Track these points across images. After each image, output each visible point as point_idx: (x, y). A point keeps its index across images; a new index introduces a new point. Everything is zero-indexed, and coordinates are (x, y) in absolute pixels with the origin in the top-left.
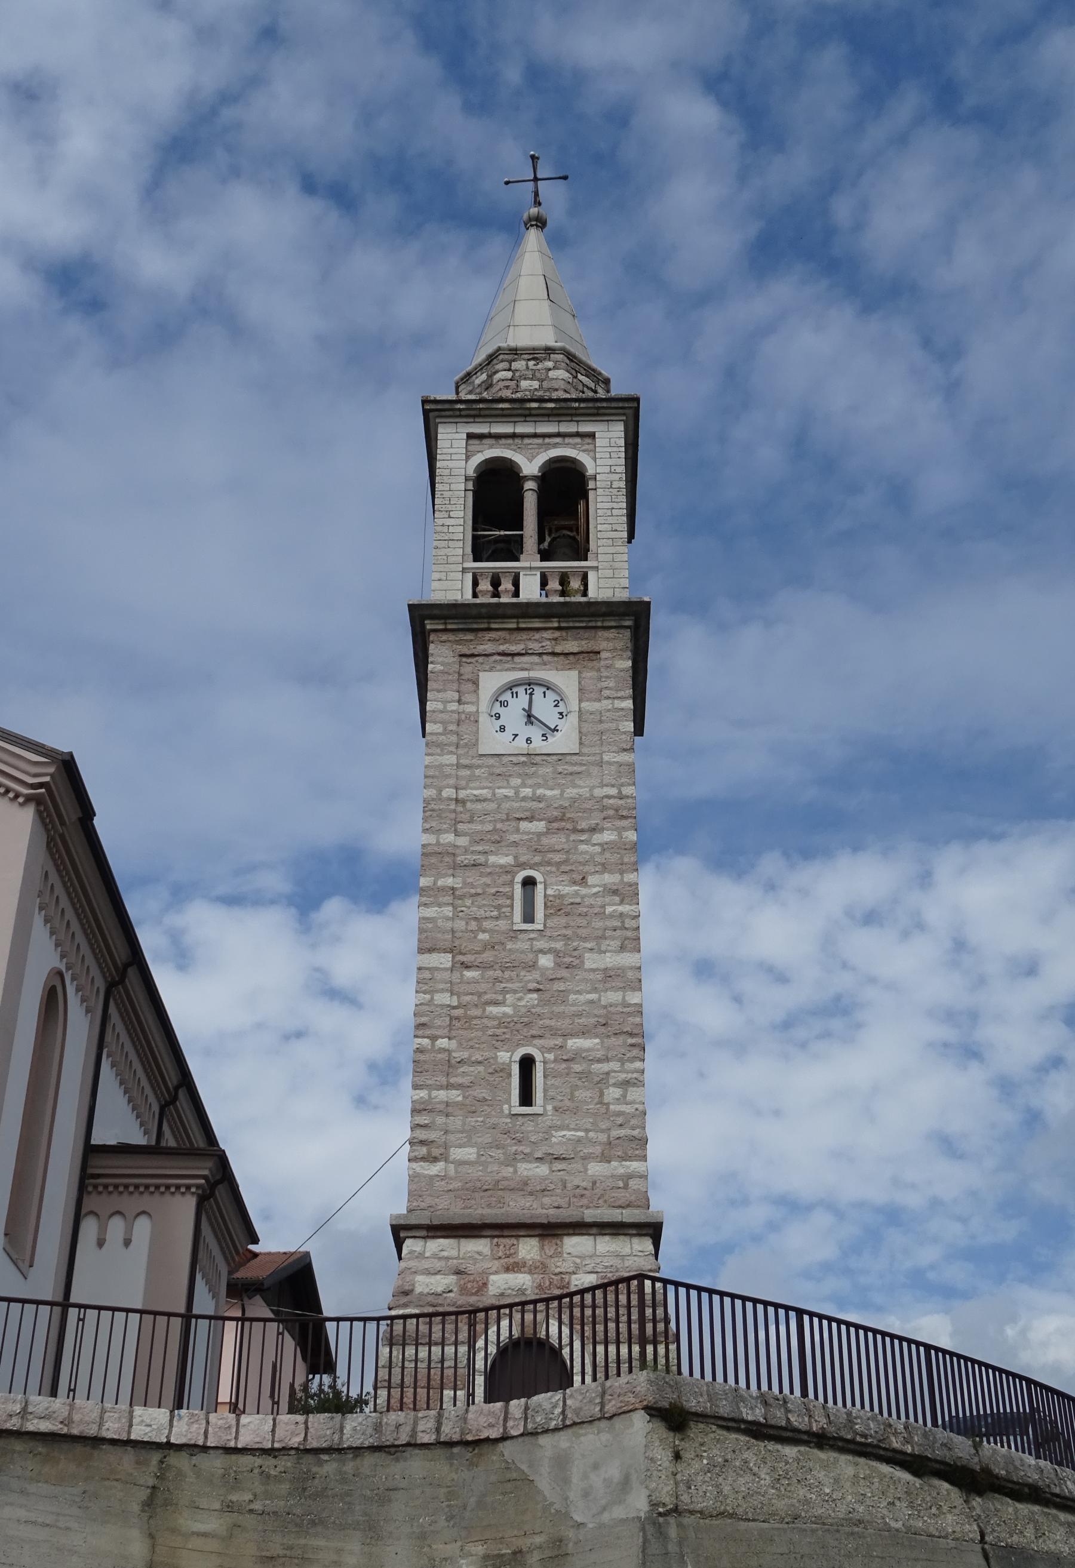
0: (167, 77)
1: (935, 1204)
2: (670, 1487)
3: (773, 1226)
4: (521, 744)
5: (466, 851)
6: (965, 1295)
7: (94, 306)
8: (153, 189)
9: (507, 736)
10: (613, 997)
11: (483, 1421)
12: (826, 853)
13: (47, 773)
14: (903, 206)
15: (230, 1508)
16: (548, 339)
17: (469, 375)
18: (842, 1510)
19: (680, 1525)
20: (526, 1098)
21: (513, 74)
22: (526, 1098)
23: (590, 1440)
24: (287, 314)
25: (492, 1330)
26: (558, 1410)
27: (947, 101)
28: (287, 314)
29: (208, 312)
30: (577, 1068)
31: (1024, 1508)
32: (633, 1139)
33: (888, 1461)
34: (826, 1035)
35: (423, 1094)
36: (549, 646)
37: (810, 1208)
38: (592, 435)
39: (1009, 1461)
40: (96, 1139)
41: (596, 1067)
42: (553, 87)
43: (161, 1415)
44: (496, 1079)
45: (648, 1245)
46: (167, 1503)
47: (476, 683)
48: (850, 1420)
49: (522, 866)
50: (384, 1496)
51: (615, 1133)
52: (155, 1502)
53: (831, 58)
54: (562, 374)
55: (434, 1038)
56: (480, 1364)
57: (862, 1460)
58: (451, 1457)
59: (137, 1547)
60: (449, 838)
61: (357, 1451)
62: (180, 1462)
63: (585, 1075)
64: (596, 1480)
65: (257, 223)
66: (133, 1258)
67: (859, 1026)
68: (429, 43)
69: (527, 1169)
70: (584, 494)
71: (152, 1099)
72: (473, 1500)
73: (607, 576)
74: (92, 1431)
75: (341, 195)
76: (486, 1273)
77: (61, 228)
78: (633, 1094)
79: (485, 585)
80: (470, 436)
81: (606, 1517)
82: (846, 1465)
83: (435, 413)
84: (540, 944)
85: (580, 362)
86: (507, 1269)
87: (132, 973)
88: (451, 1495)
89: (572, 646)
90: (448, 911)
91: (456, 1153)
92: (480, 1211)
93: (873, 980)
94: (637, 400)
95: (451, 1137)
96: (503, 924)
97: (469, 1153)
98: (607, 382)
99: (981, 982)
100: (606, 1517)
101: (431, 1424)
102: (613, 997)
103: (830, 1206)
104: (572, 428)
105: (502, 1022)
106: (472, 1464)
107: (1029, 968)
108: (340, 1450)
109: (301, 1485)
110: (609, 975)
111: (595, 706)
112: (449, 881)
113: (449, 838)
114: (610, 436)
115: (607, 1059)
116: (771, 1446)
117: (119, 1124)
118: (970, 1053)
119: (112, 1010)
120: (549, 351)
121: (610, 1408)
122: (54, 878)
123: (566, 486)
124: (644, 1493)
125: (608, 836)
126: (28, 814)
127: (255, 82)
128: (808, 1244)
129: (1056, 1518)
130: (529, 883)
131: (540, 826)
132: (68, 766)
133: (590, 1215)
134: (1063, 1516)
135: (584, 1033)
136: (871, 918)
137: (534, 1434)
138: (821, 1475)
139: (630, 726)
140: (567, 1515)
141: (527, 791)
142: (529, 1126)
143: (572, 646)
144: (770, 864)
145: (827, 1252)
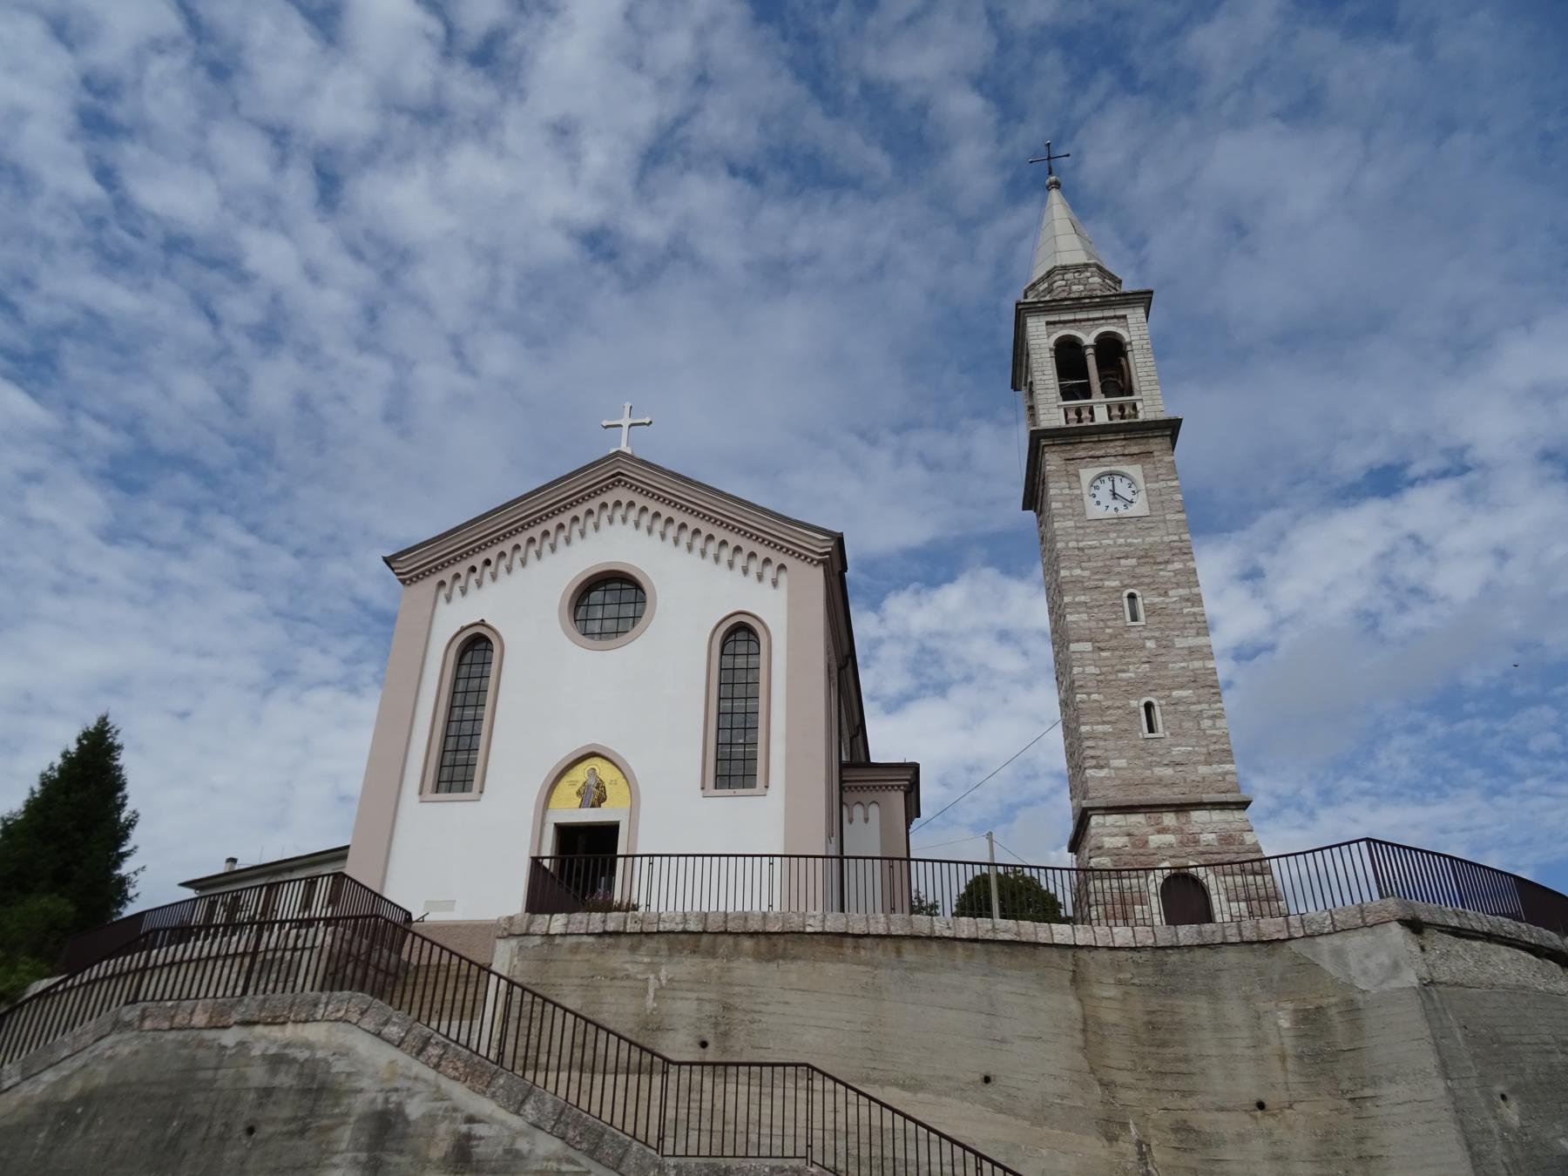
0: (644, 113)
4: (1111, 512)
7: (611, 256)
8: (640, 181)
9: (1102, 507)
10: (1197, 664)
13: (829, 546)
15: (1120, 982)
16: (1081, 258)
21: (852, 90)
22: (1151, 729)
24: (726, 251)
26: (1328, 922)
27: (1128, 81)
28: (726, 251)
32: (1224, 750)
42: (877, 96)
44: (1131, 717)
46: (1083, 980)
47: (1078, 476)
49: (1126, 587)
50: (1215, 974)
51: (1212, 747)
52: (1077, 979)
53: (1051, 59)
54: (1096, 280)
55: (1089, 694)
58: (1253, 951)
59: (1075, 1007)
60: (1078, 572)
61: (1190, 947)
62: (1083, 955)
64: (1371, 964)
65: (704, 197)
68: (799, 76)
70: (1125, 354)
72: (1276, 977)
74: (1033, 939)
76: (1146, 835)
77: (588, 211)
78: (1219, 723)
79: (1072, 415)
80: (1048, 323)
81: (1385, 987)
82: (1506, 953)
84: (1146, 634)
86: (1159, 832)
88: (1260, 973)
89: (1135, 449)
90: (1085, 617)
91: (1115, 763)
92: (1136, 798)
95: (1110, 754)
96: (1120, 623)
97: (1122, 763)
100: (1385, 987)
101: (1235, 931)
102: (1197, 664)
105: (1129, 682)
109: (1160, 968)
110: (1191, 651)
111: (1156, 486)
112: (1083, 598)
113: (1078, 572)
115: (1199, 703)
120: (1087, 266)
123: (1112, 350)
124: (1413, 973)
125: (1177, 566)
126: (820, 571)
127: (696, 110)
130: (1132, 597)
131: (1133, 561)
133: (1206, 798)
135: (1182, 687)
137: (1312, 936)
140: (1352, 985)
141: (1121, 541)
142: (1157, 745)
143: (1135, 449)
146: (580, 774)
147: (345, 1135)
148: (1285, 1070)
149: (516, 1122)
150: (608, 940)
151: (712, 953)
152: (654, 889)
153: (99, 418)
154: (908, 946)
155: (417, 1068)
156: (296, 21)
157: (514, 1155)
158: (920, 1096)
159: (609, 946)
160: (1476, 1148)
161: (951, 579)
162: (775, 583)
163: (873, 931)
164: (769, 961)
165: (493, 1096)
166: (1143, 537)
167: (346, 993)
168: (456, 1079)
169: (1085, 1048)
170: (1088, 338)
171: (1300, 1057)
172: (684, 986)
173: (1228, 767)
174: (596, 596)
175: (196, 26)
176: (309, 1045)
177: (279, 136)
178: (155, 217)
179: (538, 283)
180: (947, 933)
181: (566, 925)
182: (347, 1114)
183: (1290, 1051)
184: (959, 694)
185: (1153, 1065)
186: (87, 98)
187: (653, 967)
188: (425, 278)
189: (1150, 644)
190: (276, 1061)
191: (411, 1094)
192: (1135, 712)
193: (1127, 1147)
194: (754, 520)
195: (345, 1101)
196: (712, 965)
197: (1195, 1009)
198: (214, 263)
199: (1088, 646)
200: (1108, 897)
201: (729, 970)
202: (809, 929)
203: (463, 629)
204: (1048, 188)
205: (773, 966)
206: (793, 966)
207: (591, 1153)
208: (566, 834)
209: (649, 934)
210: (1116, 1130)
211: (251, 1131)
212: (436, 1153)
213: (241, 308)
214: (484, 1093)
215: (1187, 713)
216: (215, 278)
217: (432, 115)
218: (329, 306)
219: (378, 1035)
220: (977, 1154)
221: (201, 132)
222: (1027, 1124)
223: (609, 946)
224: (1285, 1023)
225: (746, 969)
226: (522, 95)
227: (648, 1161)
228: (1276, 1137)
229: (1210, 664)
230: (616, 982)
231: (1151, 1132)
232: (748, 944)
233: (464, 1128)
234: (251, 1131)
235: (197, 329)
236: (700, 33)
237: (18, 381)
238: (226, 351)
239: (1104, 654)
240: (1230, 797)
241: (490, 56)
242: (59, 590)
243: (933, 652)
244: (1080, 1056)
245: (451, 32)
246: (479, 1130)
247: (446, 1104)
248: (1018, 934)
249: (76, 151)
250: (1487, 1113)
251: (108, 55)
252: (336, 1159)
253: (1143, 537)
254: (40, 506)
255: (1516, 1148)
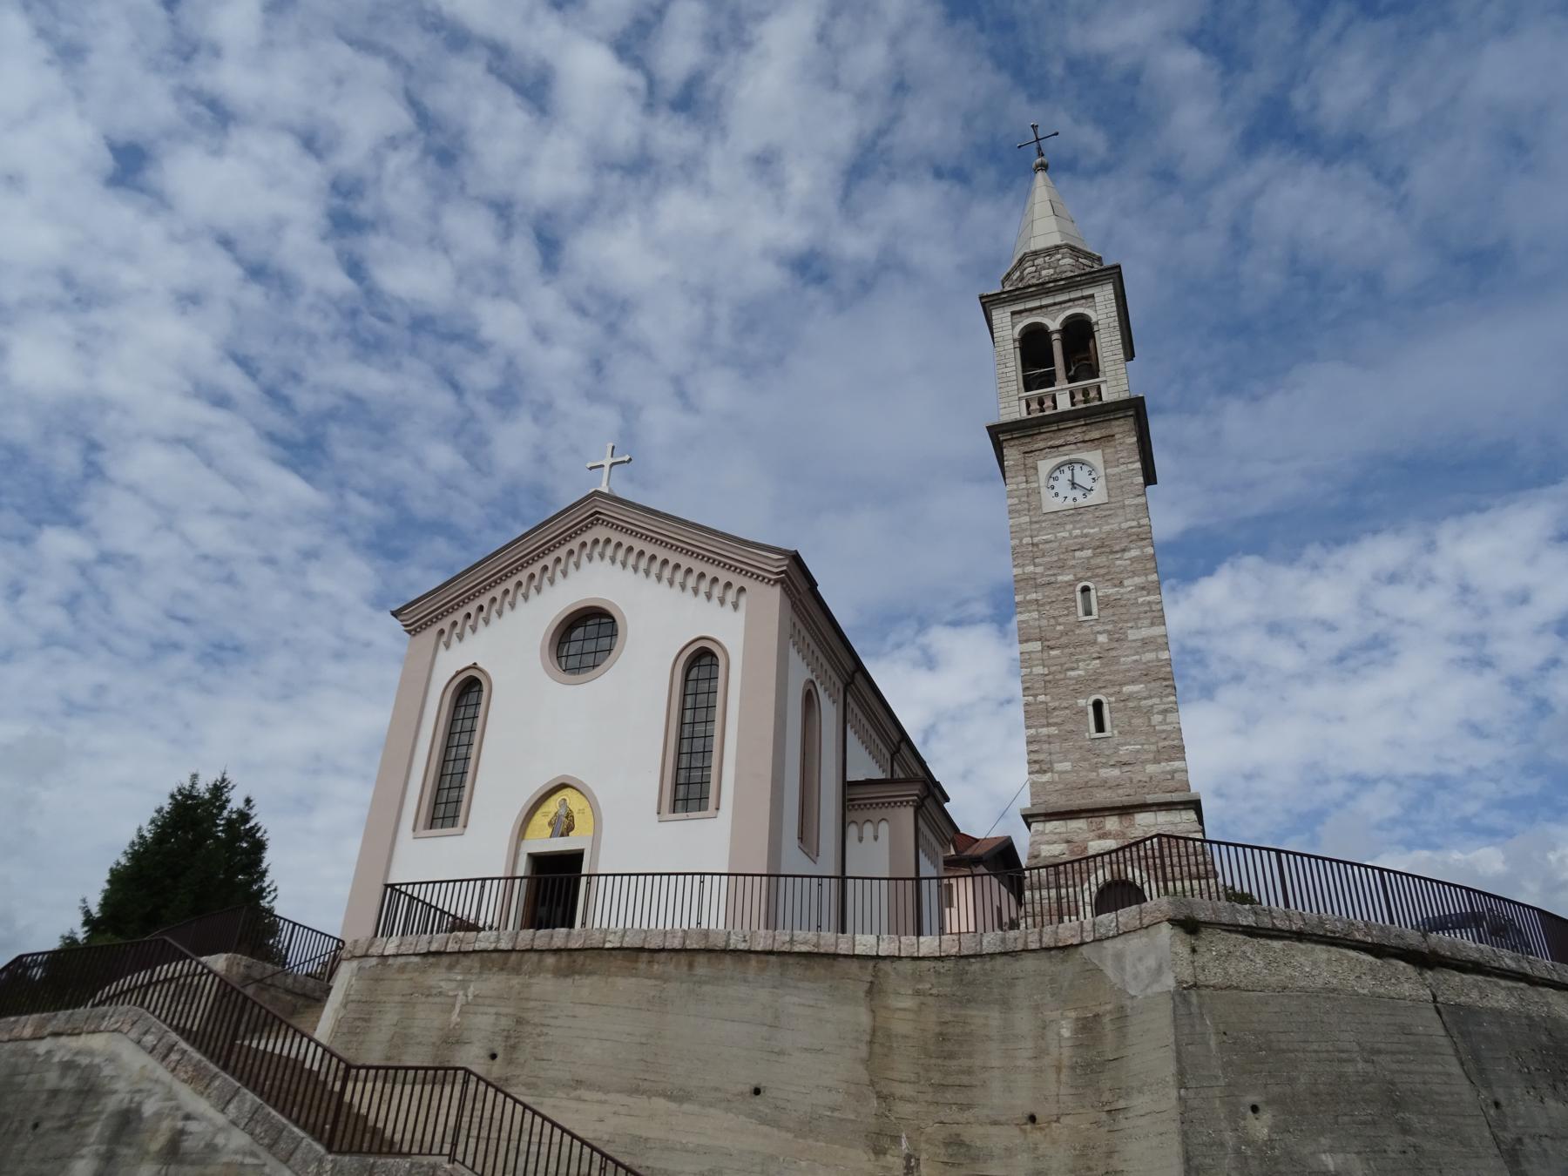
0: (841, 130)
1: (1472, 772)
2: (1190, 970)
3: (1350, 796)
4: (1070, 502)
5: (1043, 575)
6: (1509, 834)
7: (821, 279)
9: (1060, 499)
11: (1068, 933)
12: (1355, 539)
13: (784, 564)
14: (1344, 86)
15: (917, 993)
17: (1009, 275)
18: (1319, 982)
19: (1199, 996)
20: (1100, 727)
21: (1057, 69)
22: (1100, 727)
23: (1136, 942)
25: (1093, 878)
29: (889, 266)
30: (1131, 704)
31: (1469, 978)
32: (1174, 747)
33: (1354, 948)
34: (1370, 663)
35: (1033, 731)
36: (1080, 437)
37: (1375, 781)
38: (1092, 296)
39: (1453, 945)
40: (851, 777)
41: (1143, 703)
42: (1084, 69)
43: (872, 939)
45: (1192, 815)
48: (1321, 922)
49: (1080, 580)
50: (1011, 983)
51: (1161, 744)
52: (873, 991)
55: (1035, 696)
56: (1087, 899)
57: (1333, 949)
59: (864, 1018)
60: (1031, 568)
61: (992, 955)
62: (882, 965)
63: (1137, 709)
64: (1141, 968)
65: (911, 204)
66: (881, 847)
67: (1395, 654)
68: (1000, 64)
69: (1106, 773)
71: (884, 750)
73: (1114, 383)
74: (832, 950)
75: (959, 175)
76: (1086, 841)
77: (794, 235)
78: (1171, 717)
79: (1035, 406)
80: (1013, 313)
81: (1149, 992)
82: (1321, 952)
83: (989, 303)
84: (1099, 628)
85: (1079, 251)
86: (1100, 837)
87: (858, 676)
88: (1053, 981)
89: (1095, 434)
90: (1035, 615)
91: (1058, 767)
92: (1078, 802)
93: (1400, 621)
94: (1119, 267)
95: (1054, 757)
96: (1072, 619)
97: (1067, 766)
98: (1100, 259)
99: (1485, 612)
101: (1036, 937)
103: (1391, 779)
104: (1078, 294)
105: (1078, 680)
106: (1063, 961)
107: (1522, 598)
108: (981, 956)
109: (960, 977)
110: (1145, 642)
111: (1116, 470)
112: (1034, 596)
113: (1031, 568)
114: (1104, 294)
115: (1151, 697)
116: (1262, 941)
117: (864, 766)
118: (1484, 663)
119: (849, 699)
120: (1058, 247)
121: (1146, 921)
122: (799, 625)
123: (1079, 333)
124: (1172, 975)
125: (1134, 553)
126: (778, 589)
127: (895, 119)
128: (1377, 805)
129: (1497, 985)
130: (1086, 590)
131: (1089, 553)
132: (796, 558)
133: (1150, 799)
134: (1503, 983)
135: (1133, 682)
136: (1393, 579)
137: (1100, 940)
138: (1302, 960)
139: (1141, 480)
141: (1078, 532)
142: (1104, 745)
143: (1095, 434)
144: (1313, 552)
145: (1394, 811)
146: (552, 806)
147: (96, 1130)
148: (1059, 1081)
149: (221, 1119)
150: (431, 960)
151: (517, 970)
152: (605, 913)
153: (364, 494)
154: (701, 959)
155: (161, 1072)
156: (510, 98)
157: (212, 1148)
158: (686, 1107)
159: (431, 965)
160: (1195, 1162)
161: (1209, 571)
162: (736, 606)
163: (668, 945)
164: (566, 976)
165: (209, 1097)
166: (1100, 526)
167: (126, 1006)
168: (184, 1081)
169: (868, 1062)
170: (1054, 323)
171: (1073, 1068)
172: (488, 1001)
174: (578, 633)
175: (425, 119)
176: (91, 1053)
177: (502, 209)
178: (400, 301)
179: (754, 317)
180: (742, 946)
181: (399, 946)
182: (100, 1113)
183: (1066, 1062)
184: (1227, 695)
185: (936, 1078)
186: (337, 202)
187: (463, 985)
188: (645, 325)
189: (1102, 639)
190: (68, 1066)
191: (150, 1093)
192: (1083, 711)
193: (895, 1161)
194: (714, 545)
195: (103, 1101)
196: (515, 981)
197: (988, 1019)
198: (454, 337)
200: (1038, 909)
201: (529, 986)
202: (608, 945)
203: (458, 673)
204: (1036, 171)
205: (569, 981)
206: (588, 981)
207: (270, 1147)
208: (541, 862)
209: (466, 953)
210: (886, 1142)
211: (36, 1126)
212: (155, 1146)
213: (480, 375)
214: (202, 1094)
215: (1137, 709)
216: (454, 351)
217: (640, 166)
218: (557, 363)
219: (139, 1042)
220: (603, 1155)
221: (434, 217)
222: (790, 1136)
223: (431, 965)
224: (1066, 1033)
225: (545, 985)
226: (724, 132)
227: (311, 1156)
228: (1040, 1152)
230: (430, 999)
231: (923, 1146)
232: (550, 960)
233: (180, 1124)
234: (36, 1126)
235: (443, 400)
236: (895, 41)
237: (295, 469)
238: (471, 417)
239: (1053, 653)
241: (691, 101)
242: (339, 656)
243: (1194, 651)
244: (861, 1068)
245: (652, 84)
246: (192, 1126)
247: (173, 1103)
248: (817, 945)
249: (328, 250)
250: (1224, 1124)
251: (350, 158)
252: (84, 1151)
253: (1100, 526)
254: (319, 581)
255: (1254, 1164)
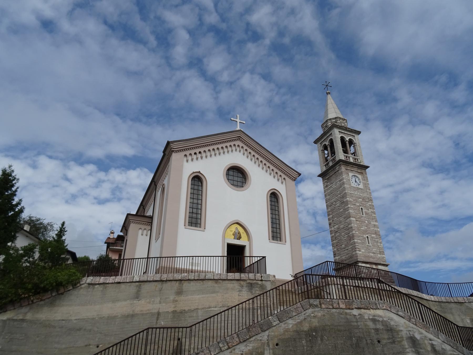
42: (160, 20)
49: (360, 206)
75: (112, 27)
77: (48, 13)
89: (359, 171)
97: (363, 251)
102: (376, 229)
113: (351, 199)
133: (382, 263)
137: (470, 302)
143: (359, 171)
161: (134, 169)
173: (384, 256)
189: (366, 222)
192: (365, 238)
199: (354, 219)
203: (194, 173)
215: (375, 241)
229: (379, 230)
240: (384, 263)
252: (408, 350)
